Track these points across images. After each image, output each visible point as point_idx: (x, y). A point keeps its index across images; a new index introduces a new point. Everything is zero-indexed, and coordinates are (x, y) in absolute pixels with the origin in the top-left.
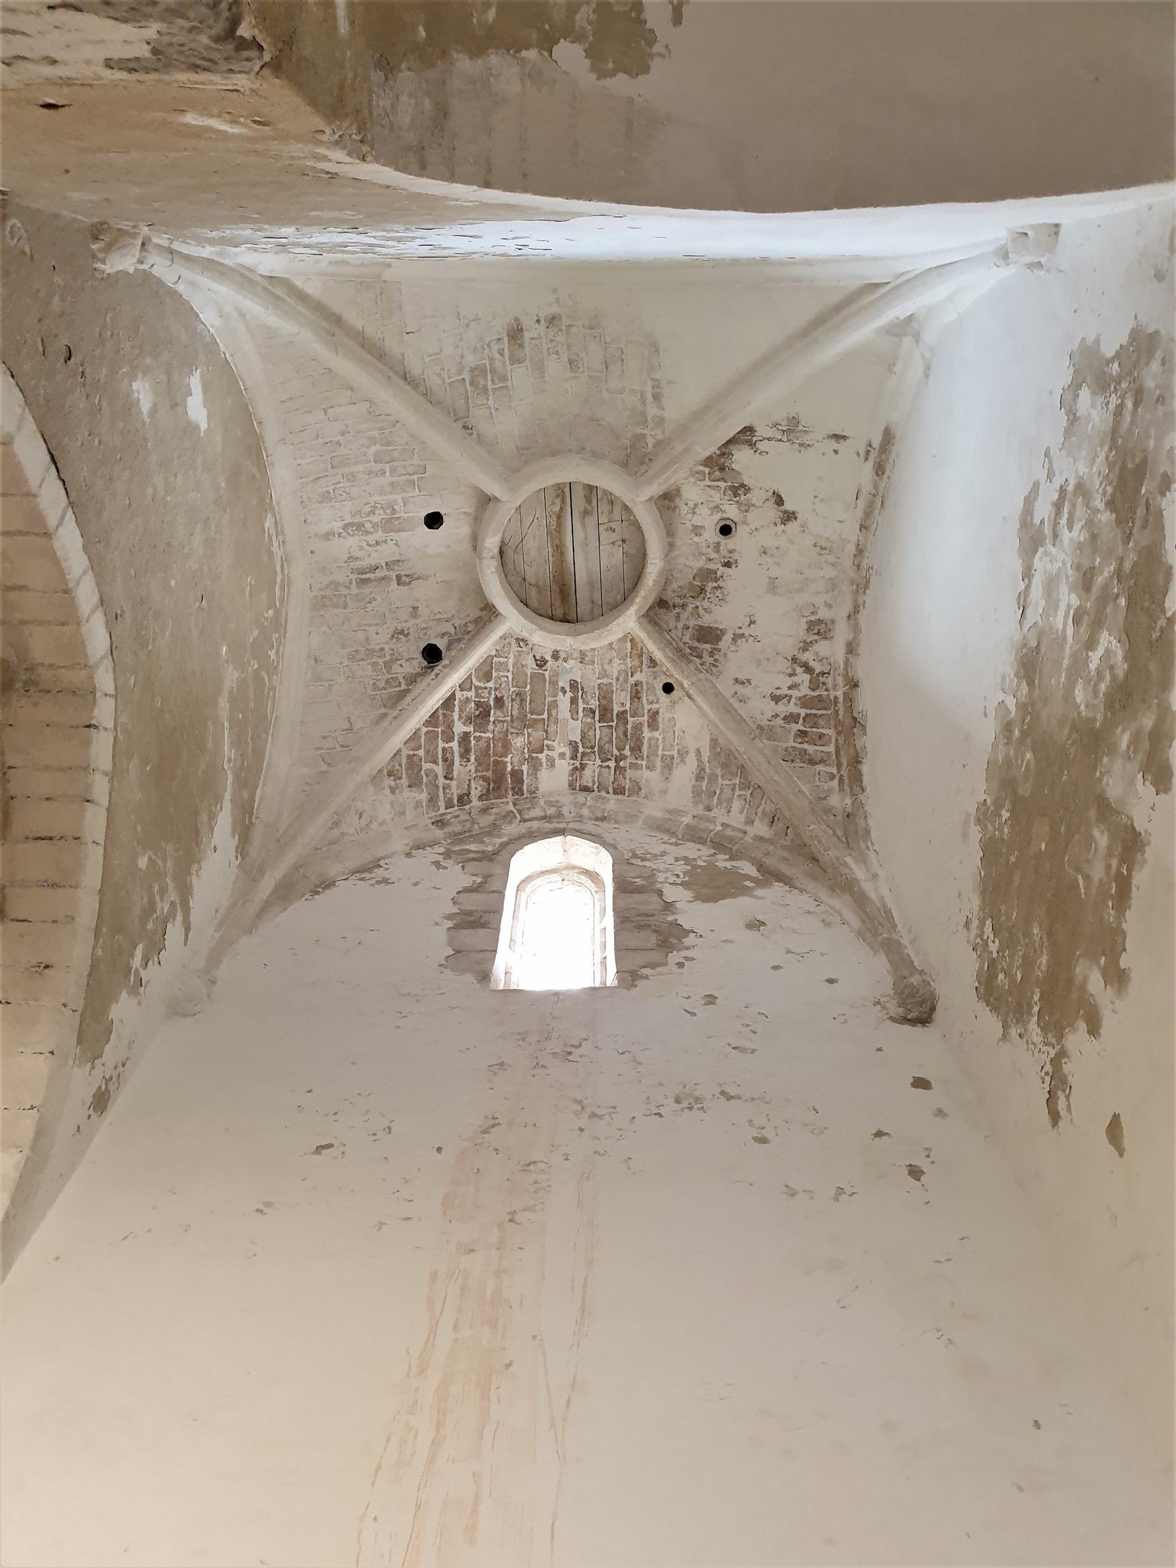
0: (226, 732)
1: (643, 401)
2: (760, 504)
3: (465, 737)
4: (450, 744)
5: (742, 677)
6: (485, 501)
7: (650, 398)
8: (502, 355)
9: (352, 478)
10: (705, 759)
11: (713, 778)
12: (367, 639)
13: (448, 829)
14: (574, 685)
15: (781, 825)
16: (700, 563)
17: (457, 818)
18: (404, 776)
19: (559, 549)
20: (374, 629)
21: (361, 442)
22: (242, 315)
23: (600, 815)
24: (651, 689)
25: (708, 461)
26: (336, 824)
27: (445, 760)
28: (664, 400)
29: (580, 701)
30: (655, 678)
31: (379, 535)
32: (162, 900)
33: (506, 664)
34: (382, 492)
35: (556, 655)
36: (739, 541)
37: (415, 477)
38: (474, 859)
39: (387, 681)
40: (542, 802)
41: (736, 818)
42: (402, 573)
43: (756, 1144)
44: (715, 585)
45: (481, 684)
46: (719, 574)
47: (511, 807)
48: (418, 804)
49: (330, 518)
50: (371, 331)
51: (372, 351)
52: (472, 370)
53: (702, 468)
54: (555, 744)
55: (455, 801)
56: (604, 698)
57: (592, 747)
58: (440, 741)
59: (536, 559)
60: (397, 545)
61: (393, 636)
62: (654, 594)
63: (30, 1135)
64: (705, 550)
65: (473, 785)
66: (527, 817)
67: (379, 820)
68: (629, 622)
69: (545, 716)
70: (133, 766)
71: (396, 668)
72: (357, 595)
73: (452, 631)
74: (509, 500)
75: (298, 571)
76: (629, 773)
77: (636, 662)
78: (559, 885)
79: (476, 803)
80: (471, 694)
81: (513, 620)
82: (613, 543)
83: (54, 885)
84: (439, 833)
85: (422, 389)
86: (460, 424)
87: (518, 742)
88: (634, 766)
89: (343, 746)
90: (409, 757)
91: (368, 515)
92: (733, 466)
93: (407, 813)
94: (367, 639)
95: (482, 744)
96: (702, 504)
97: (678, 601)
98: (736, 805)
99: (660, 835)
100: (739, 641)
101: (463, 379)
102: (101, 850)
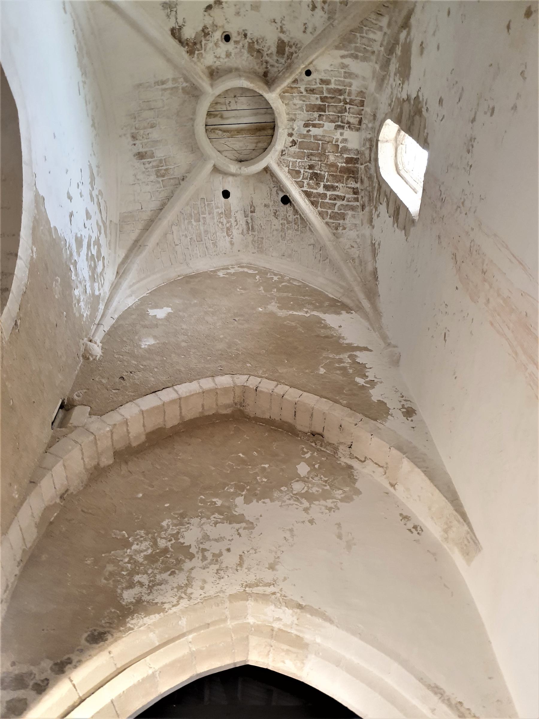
0: (295, 313)
1: (165, 90)
2: (212, 18)
3: (326, 187)
4: (328, 196)
5: (303, 28)
6: (216, 170)
7: (164, 86)
8: (150, 162)
9: (206, 232)
10: (346, 53)
11: (356, 49)
12: (277, 230)
13: (366, 204)
14: (306, 125)
15: (382, 10)
16: (245, 52)
17: (363, 198)
18: (338, 222)
19: (239, 131)
20: (273, 227)
21: (190, 228)
22: (130, 287)
23: (372, 118)
24: (309, 83)
25: (191, 52)
26: (353, 259)
27: (335, 199)
28: (164, 79)
29: (314, 122)
30: (303, 80)
31: (232, 220)
32: (344, 362)
33: (293, 162)
34: (213, 218)
35: (291, 135)
36: (233, 29)
37: (206, 203)
38: (379, 196)
39: (295, 224)
40: (363, 149)
41: (378, 36)
42: (250, 210)
43: (493, 116)
44: (256, 43)
45: (302, 176)
46: (250, 41)
47: (363, 167)
48: (353, 216)
49: (224, 242)
50: (140, 226)
51: (149, 225)
52: (158, 176)
53: (196, 56)
54: (335, 138)
55: (356, 196)
56: (313, 109)
57: (339, 117)
58: (326, 201)
59: (243, 144)
60: (237, 212)
61: (277, 218)
62: (258, 83)
63: (399, 453)
64: (239, 50)
65: (349, 186)
66: (368, 159)
67: (356, 238)
68: (273, 97)
69: (320, 142)
70: (282, 370)
71: (290, 219)
72: (258, 232)
73: (276, 188)
74: (215, 158)
75: (246, 259)
76: (353, 97)
77: (295, 90)
78: (404, 147)
79: (358, 185)
80: (306, 182)
81: (270, 160)
82: (236, 102)
83: (312, 415)
84: (367, 209)
85: (166, 201)
86: (182, 182)
87: (332, 158)
88: (349, 94)
89: (320, 250)
90: (330, 218)
91: (223, 225)
92: (193, 37)
93: (355, 222)
94: (277, 230)
95: (330, 178)
96: (215, 53)
97: (264, 65)
98: (371, 36)
99: (385, 85)
100: (284, 29)
101: (162, 181)
102: (305, 394)
